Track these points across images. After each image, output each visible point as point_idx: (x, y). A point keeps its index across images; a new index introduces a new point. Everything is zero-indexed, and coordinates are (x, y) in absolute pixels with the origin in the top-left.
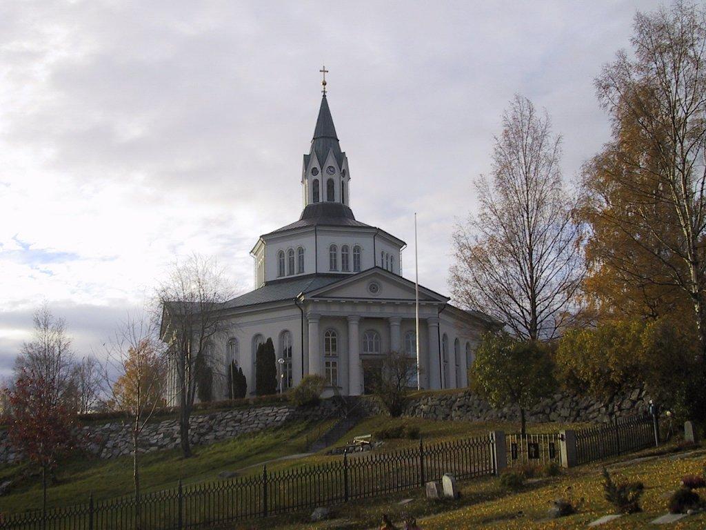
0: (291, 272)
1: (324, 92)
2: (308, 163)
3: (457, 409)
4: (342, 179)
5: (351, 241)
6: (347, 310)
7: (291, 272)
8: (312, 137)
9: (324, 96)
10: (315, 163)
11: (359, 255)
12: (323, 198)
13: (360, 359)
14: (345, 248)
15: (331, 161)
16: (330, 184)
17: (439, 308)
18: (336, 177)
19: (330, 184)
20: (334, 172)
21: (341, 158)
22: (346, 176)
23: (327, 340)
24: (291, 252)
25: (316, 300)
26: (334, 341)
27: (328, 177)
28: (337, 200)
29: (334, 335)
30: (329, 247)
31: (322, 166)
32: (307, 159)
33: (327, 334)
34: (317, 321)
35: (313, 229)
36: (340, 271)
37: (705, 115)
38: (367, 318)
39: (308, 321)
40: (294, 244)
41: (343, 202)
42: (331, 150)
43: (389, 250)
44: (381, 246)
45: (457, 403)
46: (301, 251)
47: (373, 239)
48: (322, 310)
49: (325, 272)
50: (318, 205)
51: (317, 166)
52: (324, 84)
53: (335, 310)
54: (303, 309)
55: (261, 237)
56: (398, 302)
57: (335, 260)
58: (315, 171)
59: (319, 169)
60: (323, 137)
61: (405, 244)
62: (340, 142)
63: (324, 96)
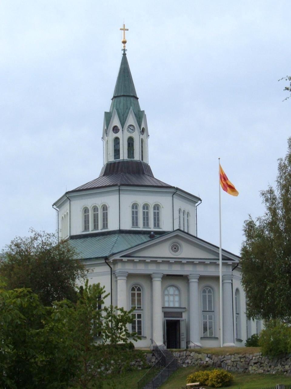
0: (96, 227)
1: (124, 50)
2: (109, 124)
3: (253, 364)
5: (151, 199)
6: (151, 269)
7: (96, 227)
8: (111, 94)
9: (124, 55)
10: (116, 122)
11: (158, 213)
12: (124, 156)
13: (163, 311)
14: (146, 207)
15: (131, 120)
16: (131, 142)
17: (233, 266)
18: (136, 136)
19: (131, 142)
20: (133, 130)
21: (140, 116)
23: (133, 295)
24: (95, 209)
25: (125, 259)
26: (139, 295)
27: (127, 135)
28: (137, 157)
29: (209, 292)
30: (131, 206)
31: (123, 125)
32: (108, 117)
33: (133, 289)
34: (125, 278)
35: (117, 188)
37: (79, 388)
38: (168, 276)
39: (116, 277)
40: (98, 201)
41: (142, 160)
42: (131, 108)
44: (179, 204)
45: (253, 361)
46: (105, 208)
47: (172, 198)
48: (130, 268)
50: (119, 163)
52: (124, 42)
53: (141, 269)
54: (112, 266)
56: (208, 262)
57: (137, 218)
58: (116, 129)
59: (119, 126)
60: (124, 96)
61: (200, 200)
63: (124, 55)
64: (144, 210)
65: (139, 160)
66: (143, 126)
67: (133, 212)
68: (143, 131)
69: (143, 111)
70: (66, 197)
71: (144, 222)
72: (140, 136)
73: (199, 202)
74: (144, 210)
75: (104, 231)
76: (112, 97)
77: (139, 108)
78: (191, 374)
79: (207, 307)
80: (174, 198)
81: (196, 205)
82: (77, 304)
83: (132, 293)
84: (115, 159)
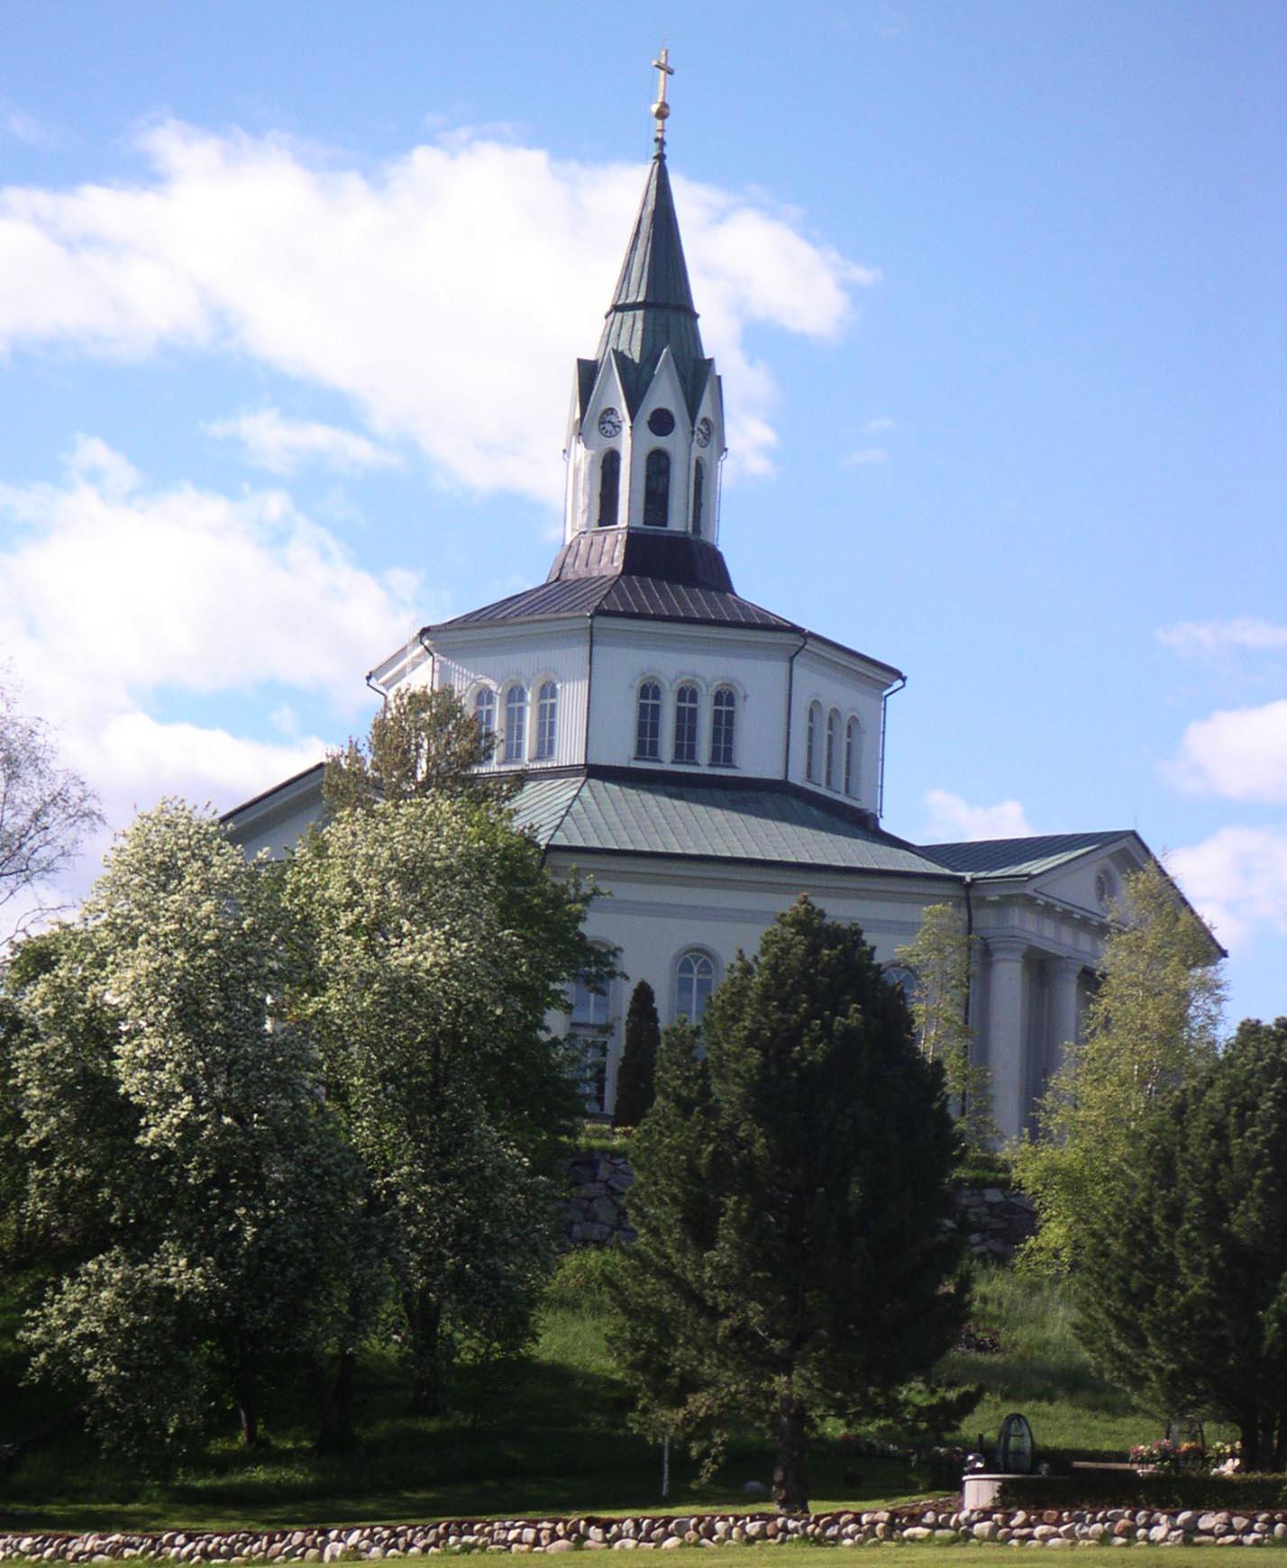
1: (661, 142)
4: (697, 451)
7: (685, 750)
11: (730, 715)
16: (657, 466)
18: (674, 443)
22: (714, 438)
28: (678, 521)
36: (703, 767)
41: (697, 529)
43: (840, 695)
47: (784, 666)
49: (618, 765)
51: (675, 406)
55: (425, 632)
61: (898, 675)
62: (700, 322)
64: (691, 705)
65: (683, 529)
66: (705, 410)
67: (643, 708)
69: (711, 361)
70: (422, 647)
71: (654, 739)
72: (690, 446)
73: (899, 683)
74: (691, 705)
75: (537, 765)
76: (608, 308)
77: (696, 350)
78: (611, 1290)
80: (794, 665)
81: (886, 693)
83: (680, 978)
84: (645, 523)
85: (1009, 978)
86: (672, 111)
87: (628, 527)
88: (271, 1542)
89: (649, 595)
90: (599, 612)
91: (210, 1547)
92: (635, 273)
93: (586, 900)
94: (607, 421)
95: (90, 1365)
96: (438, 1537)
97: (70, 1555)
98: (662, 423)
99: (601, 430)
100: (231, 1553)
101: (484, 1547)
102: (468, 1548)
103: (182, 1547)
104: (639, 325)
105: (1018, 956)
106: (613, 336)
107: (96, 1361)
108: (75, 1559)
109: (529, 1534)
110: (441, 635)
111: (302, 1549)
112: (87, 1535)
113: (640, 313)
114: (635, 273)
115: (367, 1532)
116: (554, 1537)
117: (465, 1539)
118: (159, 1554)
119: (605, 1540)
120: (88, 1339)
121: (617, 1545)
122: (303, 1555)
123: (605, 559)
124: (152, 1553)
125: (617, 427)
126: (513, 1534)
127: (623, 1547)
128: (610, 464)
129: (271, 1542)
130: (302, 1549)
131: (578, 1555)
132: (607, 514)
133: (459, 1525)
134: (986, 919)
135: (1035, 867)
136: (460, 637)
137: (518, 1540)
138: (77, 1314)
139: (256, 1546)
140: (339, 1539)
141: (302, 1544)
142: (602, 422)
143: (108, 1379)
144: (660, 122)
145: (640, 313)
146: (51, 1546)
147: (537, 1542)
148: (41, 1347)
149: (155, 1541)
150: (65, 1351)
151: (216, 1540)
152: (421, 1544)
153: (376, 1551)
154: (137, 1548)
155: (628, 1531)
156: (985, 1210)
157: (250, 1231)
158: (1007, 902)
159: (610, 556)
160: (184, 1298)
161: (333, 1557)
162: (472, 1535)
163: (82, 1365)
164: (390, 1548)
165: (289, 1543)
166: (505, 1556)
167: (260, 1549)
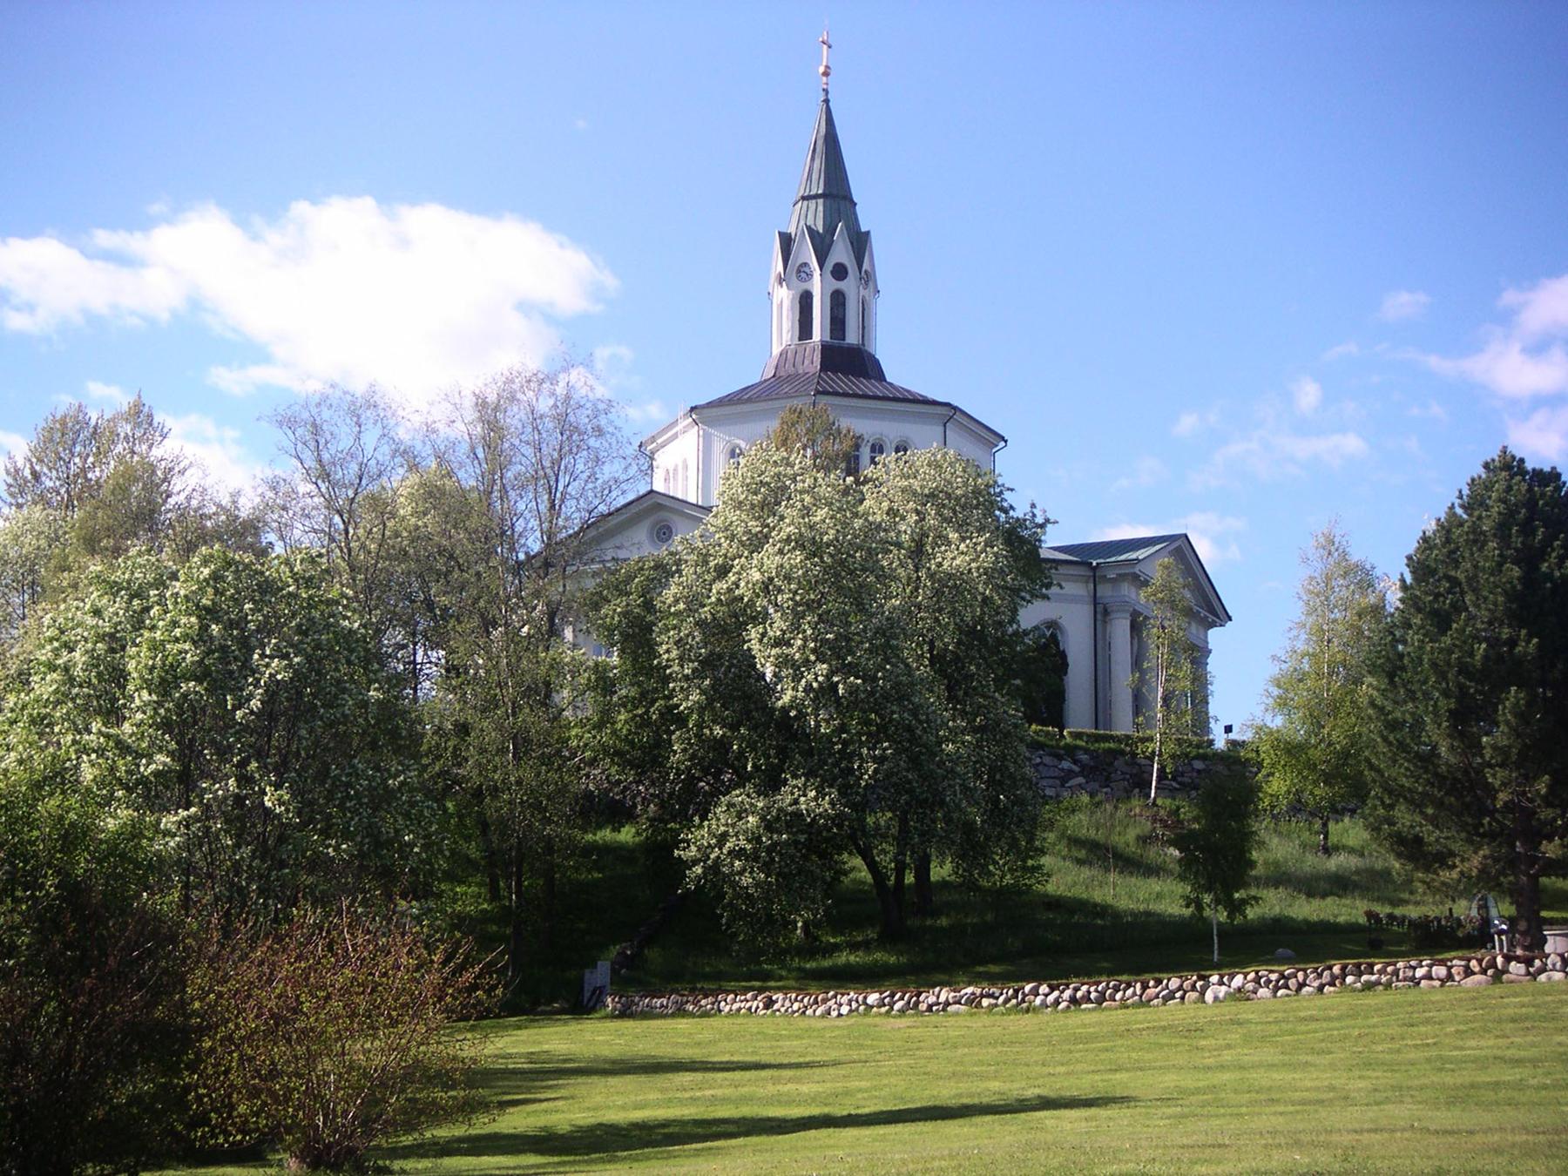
1: (826, 91)
4: (862, 292)
16: (838, 301)
18: (849, 286)
22: (871, 283)
28: (852, 338)
41: (863, 344)
47: (941, 429)
55: (693, 409)
66: (866, 266)
68: (867, 279)
69: (868, 233)
79: (1216, 946)
82: (131, 687)
85: (1120, 629)
86: (832, 72)
87: (821, 341)
88: (1145, 987)
89: (854, 384)
90: (818, 393)
91: (1079, 994)
92: (815, 176)
93: (1042, 526)
94: (803, 272)
95: (741, 873)
96: (1334, 977)
97: (923, 1007)
98: (840, 272)
99: (798, 277)
100: (1102, 998)
101: (1388, 985)
102: (1369, 986)
103: (1046, 995)
104: (821, 208)
105: (1128, 615)
106: (803, 217)
107: (745, 870)
108: (930, 1008)
109: (1440, 971)
110: (705, 411)
111: (1181, 993)
112: (937, 989)
113: (821, 201)
114: (815, 176)
115: (1252, 975)
116: (1468, 972)
117: (1365, 978)
118: (1023, 1001)
119: (1528, 973)
120: (737, 853)
121: (1543, 977)
122: (1182, 998)
123: (806, 362)
124: (1014, 1001)
125: (810, 275)
126: (1420, 972)
127: (1549, 978)
128: (805, 301)
129: (1145, 987)
130: (1181, 993)
131: (1498, 990)
132: (805, 330)
133: (1358, 966)
134: (1105, 591)
135: (1141, 554)
136: (715, 411)
137: (1429, 977)
138: (725, 836)
139: (1130, 991)
140: (1221, 983)
141: (1180, 988)
142: (799, 271)
143: (757, 885)
144: (824, 79)
145: (821, 201)
146: (902, 998)
147: (1450, 977)
148: (695, 862)
149: (1016, 992)
150: (715, 868)
151: (1084, 988)
152: (1316, 984)
153: (1263, 992)
154: (997, 998)
155: (1554, 965)
156: (1195, 774)
157: (872, 767)
158: (1121, 577)
159: (812, 363)
160: (813, 820)
161: (1216, 998)
162: (1372, 974)
163: (732, 874)
164: (1280, 988)
165: (1167, 987)
166: (1415, 991)
167: (1134, 994)
